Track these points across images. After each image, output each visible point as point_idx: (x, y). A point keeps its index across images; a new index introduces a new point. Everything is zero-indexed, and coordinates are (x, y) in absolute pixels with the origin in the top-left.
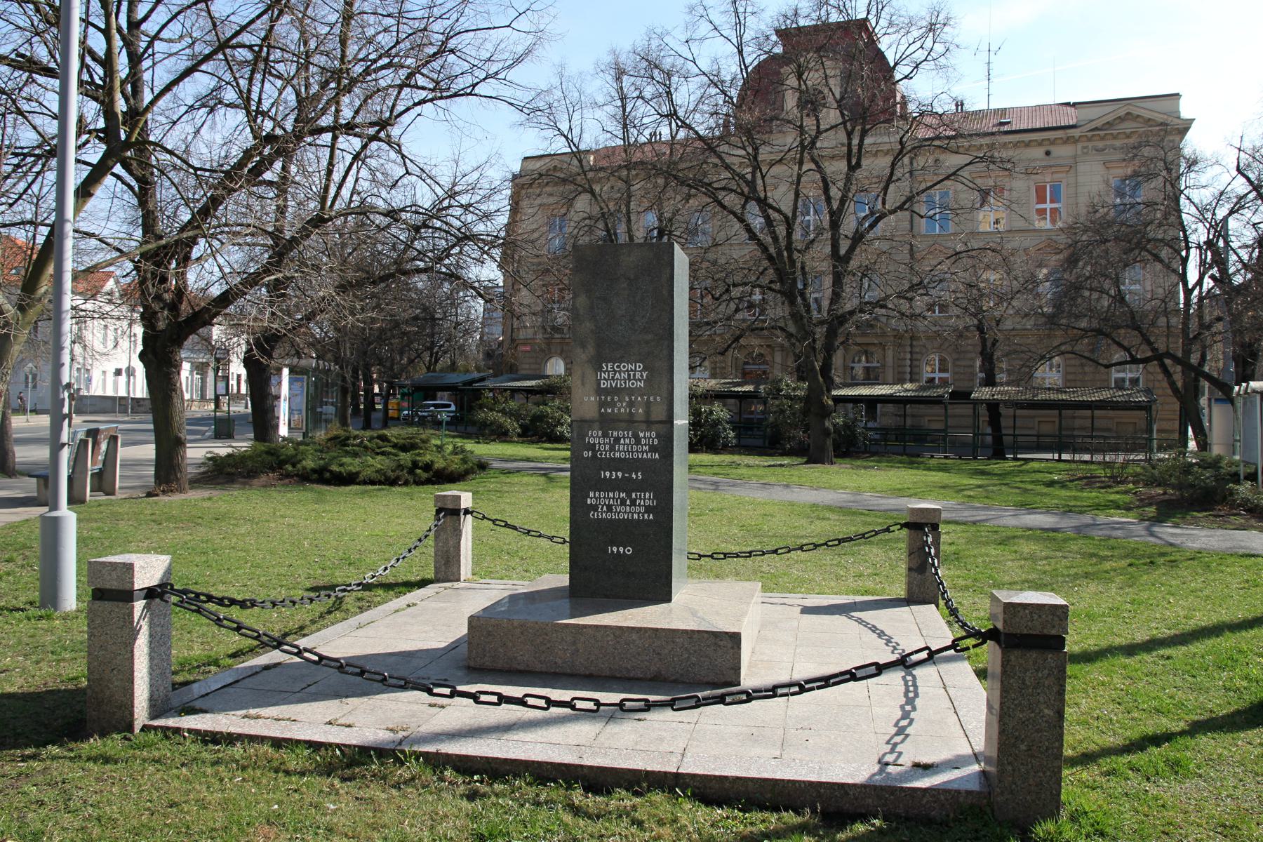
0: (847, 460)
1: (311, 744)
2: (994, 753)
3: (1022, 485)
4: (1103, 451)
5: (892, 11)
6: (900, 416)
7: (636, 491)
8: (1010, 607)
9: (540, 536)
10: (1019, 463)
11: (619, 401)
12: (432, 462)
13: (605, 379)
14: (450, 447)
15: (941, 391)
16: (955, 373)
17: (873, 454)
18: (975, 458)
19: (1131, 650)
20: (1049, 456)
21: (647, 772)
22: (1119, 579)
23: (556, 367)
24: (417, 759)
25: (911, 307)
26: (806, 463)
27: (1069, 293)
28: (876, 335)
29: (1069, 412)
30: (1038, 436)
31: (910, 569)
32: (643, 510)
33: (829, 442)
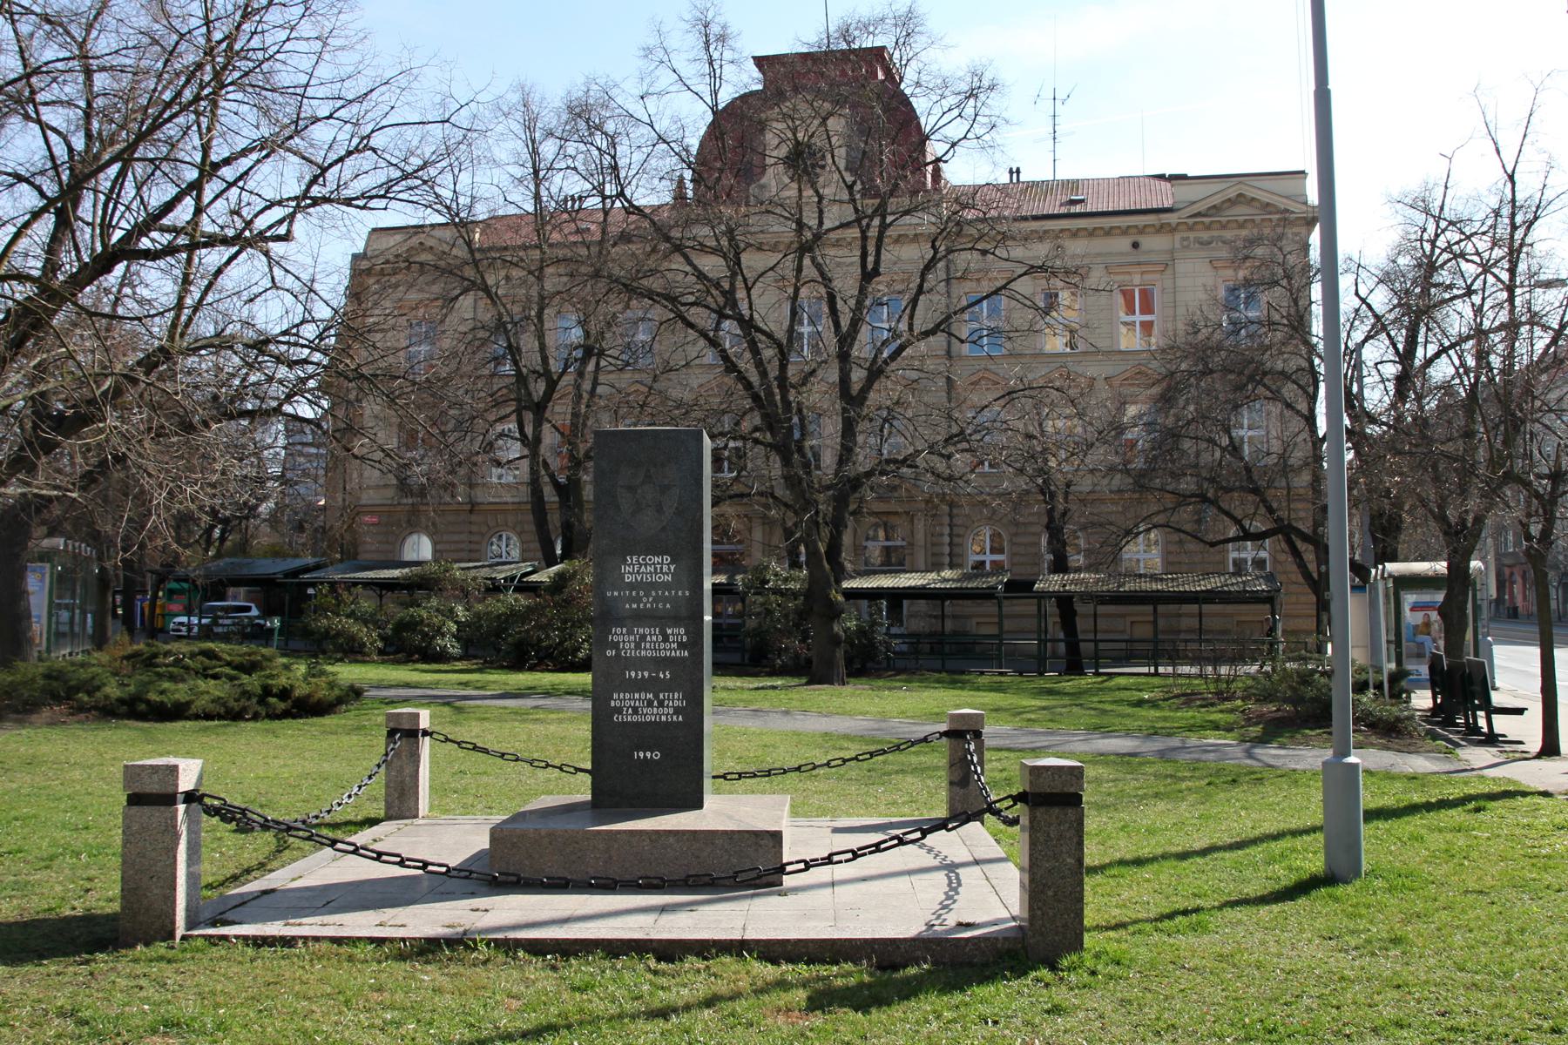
0: (864, 680)
1: (372, 940)
2: (1026, 915)
3: (1101, 706)
4: (1216, 661)
5: (921, 65)
6: (935, 617)
7: (664, 691)
8: (1036, 771)
10: (1100, 679)
11: (645, 596)
12: (291, 686)
15: (992, 581)
16: (1013, 555)
17: (899, 672)
18: (1041, 674)
19: (1184, 856)
20: (1145, 670)
21: (714, 941)
22: (1194, 797)
23: (421, 548)
24: (488, 945)
25: (949, 467)
26: (808, 684)
27: (1168, 440)
28: (900, 500)
29: (1172, 608)
31: (951, 783)
33: (840, 654)
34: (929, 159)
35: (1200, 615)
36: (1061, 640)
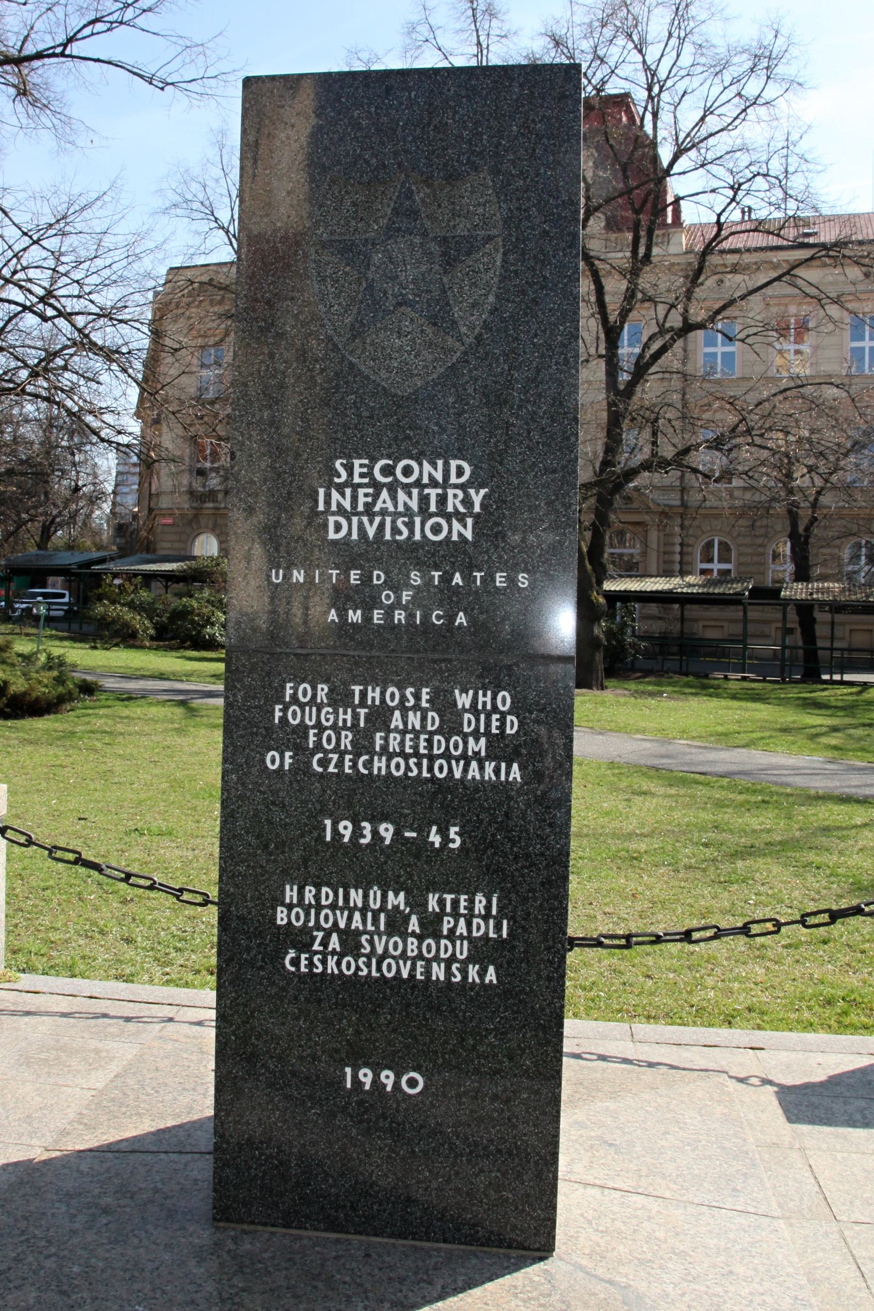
7: (442, 887)
9: (151, 888)
13: (341, 511)
14: (43, 658)
15: (738, 587)
16: (739, 564)
30: (850, 650)
32: (463, 951)
34: (670, 199)
35: (833, 623)
36: (799, 648)
